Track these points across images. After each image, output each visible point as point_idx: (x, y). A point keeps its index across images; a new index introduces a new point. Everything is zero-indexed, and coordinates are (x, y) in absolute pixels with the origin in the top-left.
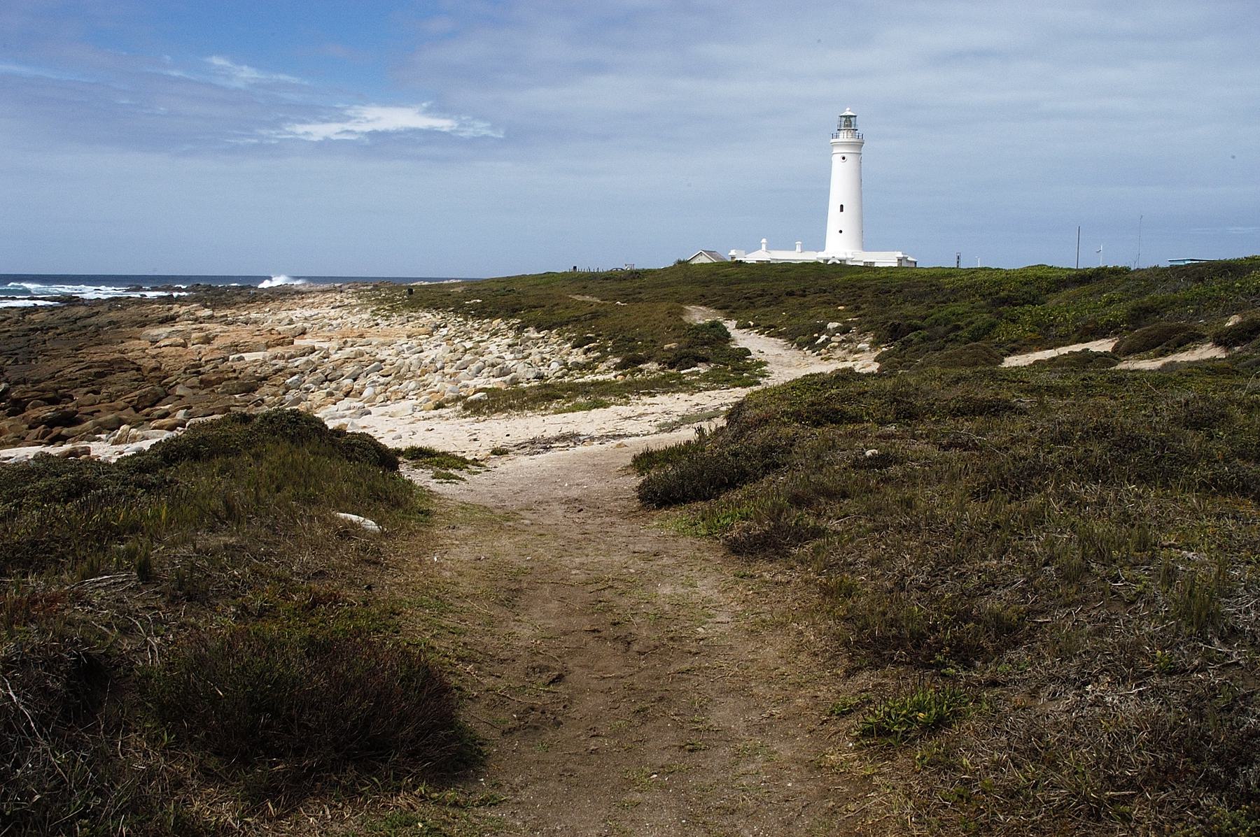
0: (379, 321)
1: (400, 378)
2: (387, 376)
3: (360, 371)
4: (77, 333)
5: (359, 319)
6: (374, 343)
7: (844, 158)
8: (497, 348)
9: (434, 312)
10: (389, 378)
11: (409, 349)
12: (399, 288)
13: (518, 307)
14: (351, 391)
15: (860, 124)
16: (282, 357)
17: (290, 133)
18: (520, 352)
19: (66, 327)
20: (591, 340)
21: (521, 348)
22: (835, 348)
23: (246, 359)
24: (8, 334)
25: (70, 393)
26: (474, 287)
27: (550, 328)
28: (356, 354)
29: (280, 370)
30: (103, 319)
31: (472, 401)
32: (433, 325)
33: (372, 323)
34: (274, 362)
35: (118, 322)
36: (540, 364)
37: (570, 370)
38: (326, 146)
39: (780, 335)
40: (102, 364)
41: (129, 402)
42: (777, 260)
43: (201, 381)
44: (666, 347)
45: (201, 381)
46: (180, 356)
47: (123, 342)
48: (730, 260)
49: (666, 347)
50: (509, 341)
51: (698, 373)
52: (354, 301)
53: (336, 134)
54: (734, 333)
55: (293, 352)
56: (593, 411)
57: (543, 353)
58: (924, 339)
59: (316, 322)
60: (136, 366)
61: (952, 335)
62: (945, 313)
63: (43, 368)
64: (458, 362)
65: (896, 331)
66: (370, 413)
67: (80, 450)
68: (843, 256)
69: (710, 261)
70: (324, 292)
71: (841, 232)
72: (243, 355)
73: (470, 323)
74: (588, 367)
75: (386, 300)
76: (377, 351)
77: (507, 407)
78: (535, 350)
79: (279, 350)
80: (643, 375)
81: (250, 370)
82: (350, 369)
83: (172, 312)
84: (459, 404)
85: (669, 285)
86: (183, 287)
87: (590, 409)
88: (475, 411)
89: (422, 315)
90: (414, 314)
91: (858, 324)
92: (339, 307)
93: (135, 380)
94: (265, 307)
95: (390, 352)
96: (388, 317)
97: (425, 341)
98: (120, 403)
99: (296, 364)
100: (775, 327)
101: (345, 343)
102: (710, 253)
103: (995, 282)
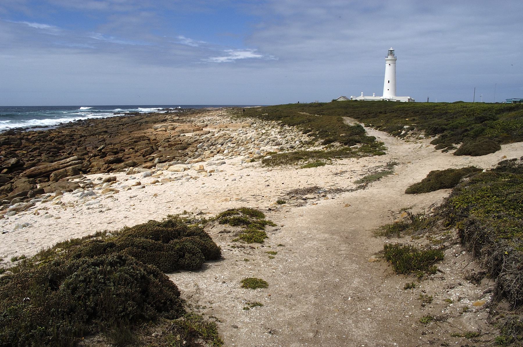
0: (233, 121)
1: (238, 145)
2: (234, 144)
3: (224, 142)
4: (134, 125)
5: (226, 121)
6: (231, 130)
7: (390, 65)
8: (274, 132)
9: (252, 118)
10: (234, 145)
11: (242, 133)
12: (240, 109)
13: (281, 116)
14: (220, 151)
15: (395, 53)
16: (198, 135)
17: (211, 60)
18: (283, 135)
19: (132, 123)
20: (309, 131)
21: (283, 133)
22: (409, 136)
23: (186, 135)
24: (113, 126)
25: (123, 149)
26: (265, 109)
27: (293, 126)
28: (223, 135)
29: (197, 141)
30: (144, 120)
31: (266, 159)
32: (251, 123)
33: (230, 122)
34: (195, 137)
35: (148, 121)
36: (291, 140)
37: (304, 144)
38: (222, 64)
39: (384, 130)
40: (137, 138)
41: (142, 153)
42: (366, 99)
43: (169, 145)
44: (341, 135)
45: (169, 145)
46: (164, 134)
47: (147, 129)
48: (350, 99)
49: (341, 135)
50: (278, 130)
51: (357, 148)
52: (225, 114)
53: (225, 60)
54: (366, 129)
55: (202, 133)
56: (318, 167)
57: (291, 135)
58: (452, 135)
59: (212, 121)
60: (148, 138)
61: (465, 134)
62: (456, 123)
63: (117, 140)
64: (260, 138)
65: (436, 130)
66: (225, 163)
67: (112, 178)
68: (389, 98)
69: (344, 100)
70: (216, 110)
71: (388, 90)
72: (185, 134)
73: (264, 122)
74: (310, 143)
75: (236, 113)
76: (231, 133)
77: (280, 163)
78: (288, 134)
79: (198, 132)
80: (334, 148)
81: (186, 140)
82: (220, 141)
83: (166, 118)
84: (260, 160)
85: (332, 108)
86: (172, 109)
87: (316, 166)
88: (267, 164)
89: (247, 119)
90: (245, 119)
91: (417, 127)
92: (220, 116)
93: (147, 144)
94: (197, 115)
95: (236, 134)
96: (236, 120)
97: (248, 129)
98: (138, 154)
99: (203, 138)
100: (381, 127)
101: (221, 129)
102: (344, 97)
103: (471, 110)
